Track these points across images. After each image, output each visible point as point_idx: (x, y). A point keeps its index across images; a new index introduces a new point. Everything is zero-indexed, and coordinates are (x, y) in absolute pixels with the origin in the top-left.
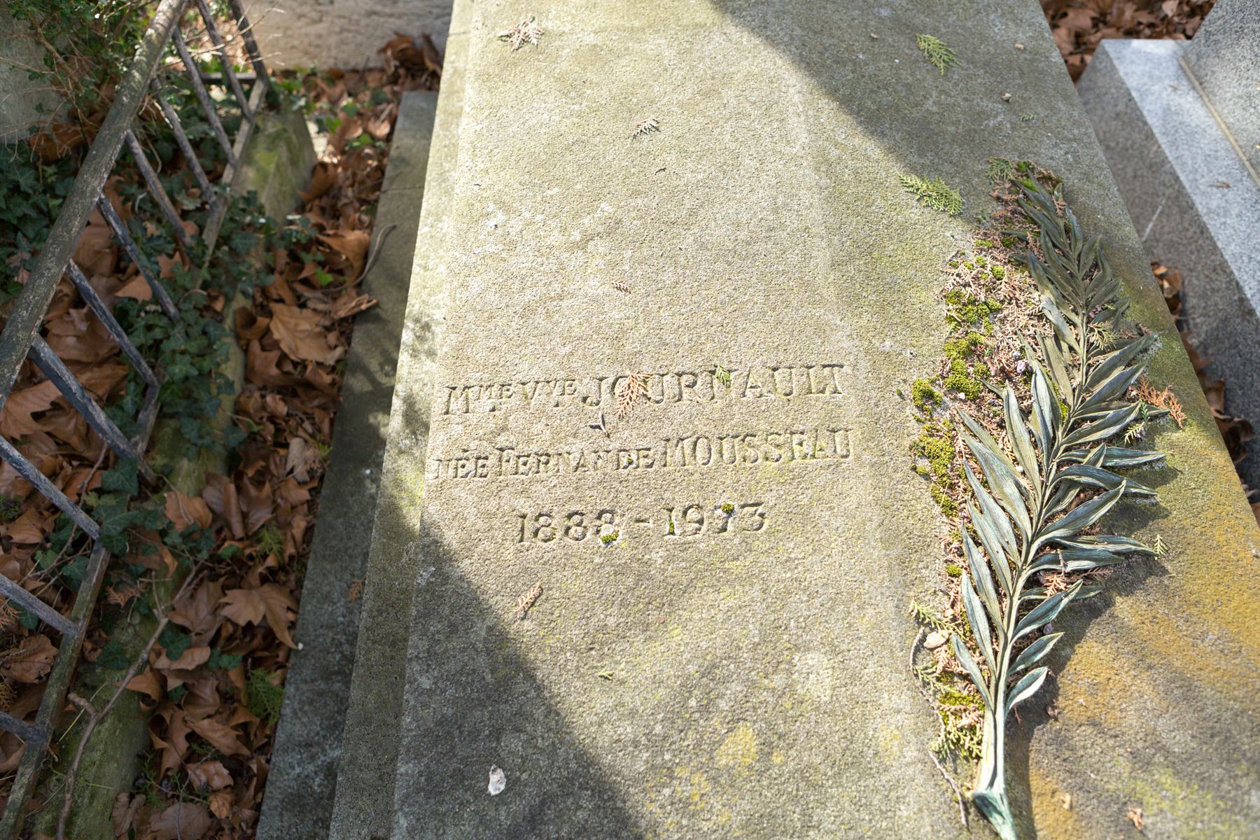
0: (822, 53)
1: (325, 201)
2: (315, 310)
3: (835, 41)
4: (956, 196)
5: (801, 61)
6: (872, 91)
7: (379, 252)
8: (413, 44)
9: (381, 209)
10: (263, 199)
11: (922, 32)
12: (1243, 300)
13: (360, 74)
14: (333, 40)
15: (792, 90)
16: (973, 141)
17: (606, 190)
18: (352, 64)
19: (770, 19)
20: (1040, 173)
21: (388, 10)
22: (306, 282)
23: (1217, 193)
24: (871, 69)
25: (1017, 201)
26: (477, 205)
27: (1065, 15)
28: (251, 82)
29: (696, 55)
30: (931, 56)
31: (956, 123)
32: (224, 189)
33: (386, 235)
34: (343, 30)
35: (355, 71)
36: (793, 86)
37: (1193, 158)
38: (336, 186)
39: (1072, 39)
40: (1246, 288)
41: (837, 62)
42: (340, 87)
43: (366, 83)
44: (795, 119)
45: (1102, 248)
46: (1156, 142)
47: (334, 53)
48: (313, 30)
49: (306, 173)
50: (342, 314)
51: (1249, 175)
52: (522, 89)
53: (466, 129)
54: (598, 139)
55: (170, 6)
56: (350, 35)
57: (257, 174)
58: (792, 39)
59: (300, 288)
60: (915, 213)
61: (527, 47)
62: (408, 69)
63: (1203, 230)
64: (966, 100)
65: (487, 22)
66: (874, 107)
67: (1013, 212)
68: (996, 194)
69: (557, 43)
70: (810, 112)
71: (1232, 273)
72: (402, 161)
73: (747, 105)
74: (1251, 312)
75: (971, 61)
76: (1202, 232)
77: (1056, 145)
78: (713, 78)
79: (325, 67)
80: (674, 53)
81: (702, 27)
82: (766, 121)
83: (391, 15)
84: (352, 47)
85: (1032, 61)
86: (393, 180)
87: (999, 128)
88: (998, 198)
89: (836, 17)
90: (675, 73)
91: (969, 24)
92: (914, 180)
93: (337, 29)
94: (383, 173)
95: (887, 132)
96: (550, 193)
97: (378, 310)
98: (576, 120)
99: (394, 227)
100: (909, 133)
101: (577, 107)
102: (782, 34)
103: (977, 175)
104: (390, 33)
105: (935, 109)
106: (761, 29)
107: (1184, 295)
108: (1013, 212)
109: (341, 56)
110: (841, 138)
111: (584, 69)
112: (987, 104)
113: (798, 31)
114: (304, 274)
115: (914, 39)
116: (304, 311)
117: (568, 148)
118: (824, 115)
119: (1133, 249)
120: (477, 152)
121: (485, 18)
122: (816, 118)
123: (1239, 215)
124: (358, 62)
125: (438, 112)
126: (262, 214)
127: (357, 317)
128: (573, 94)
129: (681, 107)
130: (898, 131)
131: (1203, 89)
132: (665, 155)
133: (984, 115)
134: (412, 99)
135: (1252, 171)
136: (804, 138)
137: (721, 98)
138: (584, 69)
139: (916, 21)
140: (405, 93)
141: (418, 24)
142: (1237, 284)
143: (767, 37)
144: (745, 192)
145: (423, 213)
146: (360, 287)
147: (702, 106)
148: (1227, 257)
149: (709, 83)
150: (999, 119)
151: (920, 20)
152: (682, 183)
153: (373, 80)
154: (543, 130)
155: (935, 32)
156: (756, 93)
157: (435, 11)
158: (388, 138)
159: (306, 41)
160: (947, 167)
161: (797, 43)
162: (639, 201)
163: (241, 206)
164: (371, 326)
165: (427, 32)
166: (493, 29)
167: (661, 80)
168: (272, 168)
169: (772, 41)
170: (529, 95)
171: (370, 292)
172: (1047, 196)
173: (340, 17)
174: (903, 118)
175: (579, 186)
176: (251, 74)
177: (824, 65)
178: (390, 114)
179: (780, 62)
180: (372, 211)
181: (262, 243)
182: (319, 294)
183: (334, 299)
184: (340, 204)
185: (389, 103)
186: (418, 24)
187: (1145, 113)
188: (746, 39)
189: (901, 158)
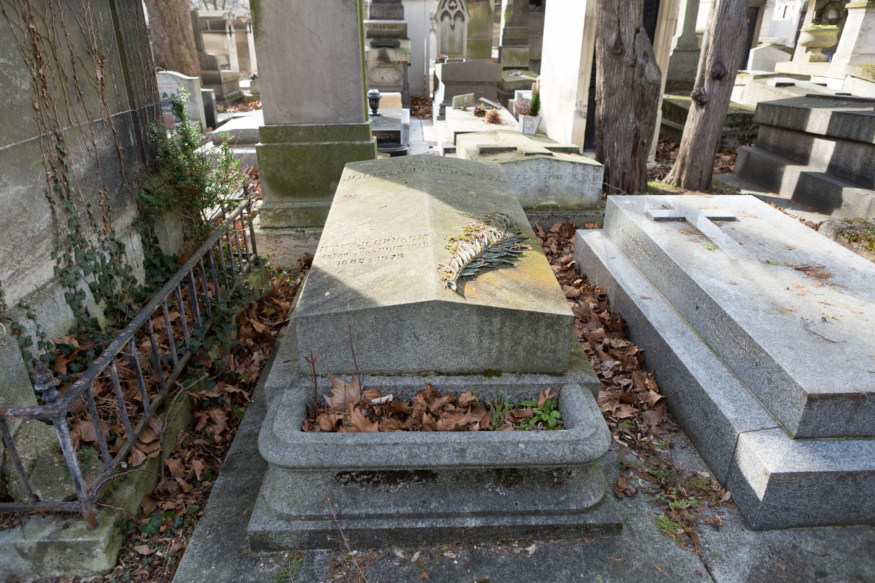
14: (280, 257)
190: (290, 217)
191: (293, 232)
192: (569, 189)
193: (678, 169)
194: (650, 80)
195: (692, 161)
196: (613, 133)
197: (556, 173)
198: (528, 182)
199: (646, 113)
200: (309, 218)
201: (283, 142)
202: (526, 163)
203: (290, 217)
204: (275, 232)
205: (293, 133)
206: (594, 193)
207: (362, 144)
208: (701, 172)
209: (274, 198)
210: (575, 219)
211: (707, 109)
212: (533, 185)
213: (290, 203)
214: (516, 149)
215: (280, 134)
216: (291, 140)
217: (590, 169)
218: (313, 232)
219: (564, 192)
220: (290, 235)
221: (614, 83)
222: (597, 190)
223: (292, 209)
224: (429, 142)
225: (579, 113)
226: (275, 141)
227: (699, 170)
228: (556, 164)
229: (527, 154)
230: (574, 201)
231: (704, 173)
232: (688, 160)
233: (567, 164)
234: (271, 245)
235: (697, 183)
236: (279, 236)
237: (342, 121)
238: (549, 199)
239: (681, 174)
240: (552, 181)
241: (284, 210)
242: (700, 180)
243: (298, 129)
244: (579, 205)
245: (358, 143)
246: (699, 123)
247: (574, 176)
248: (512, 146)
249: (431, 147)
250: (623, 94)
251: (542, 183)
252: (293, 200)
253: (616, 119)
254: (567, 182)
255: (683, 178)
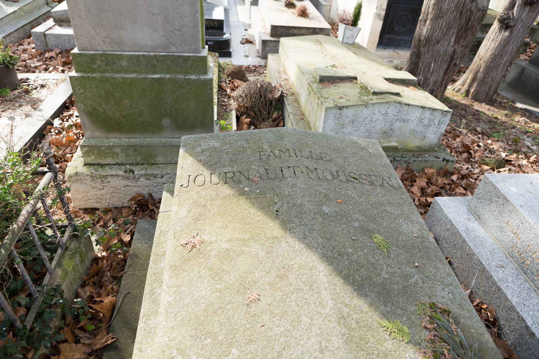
0: (332, 251)
1: (96, 279)
2: (84, 344)
3: (337, 243)
4: (406, 330)
5: (324, 256)
6: (357, 270)
7: (120, 308)
8: (144, 197)
9: (123, 282)
10: (64, 287)
11: (374, 233)
12: (527, 327)
13: (119, 209)
14: (108, 196)
15: (321, 274)
16: (407, 293)
17: (234, 340)
18: (116, 205)
19: (307, 234)
20: (441, 308)
21: (134, 185)
22: (82, 329)
23: (501, 271)
24: (355, 257)
25: (435, 328)
26: (167, 352)
27: (415, 181)
28: (66, 227)
29: (274, 254)
30: (380, 246)
31: (397, 283)
32: (43, 288)
33: (125, 297)
34: (113, 192)
35: (116, 208)
36: (322, 272)
37: (486, 253)
38: (102, 271)
39: (420, 190)
40: (527, 321)
41: (339, 255)
42: (110, 215)
43: (122, 213)
44: (325, 291)
45: (479, 351)
46: (468, 245)
47: (108, 201)
48: (99, 193)
49: (88, 263)
50: (98, 347)
51: (511, 261)
52: (192, 275)
53: (165, 297)
54: (230, 306)
55: (28, 211)
56: (116, 194)
57: (63, 273)
58: (318, 244)
59: (77, 332)
60: (389, 344)
61: (195, 250)
62: (141, 208)
63: (499, 289)
64: (399, 268)
65: (176, 236)
66: (360, 279)
67: (435, 336)
68: (423, 325)
69: (209, 248)
70: (331, 287)
71: (518, 313)
72: (135, 256)
73: (301, 283)
74: (533, 334)
75: (397, 246)
76: (499, 290)
77: (443, 289)
78: (284, 268)
79: (104, 207)
80: (264, 253)
81: (277, 238)
82: (311, 293)
83: (135, 186)
84: (117, 199)
85: (422, 242)
86: (130, 266)
87: (416, 283)
88: (426, 328)
89: (336, 230)
90: (266, 265)
91: (392, 226)
92: (385, 323)
93: (111, 192)
94: (126, 261)
95: (368, 293)
96: (206, 342)
97: (117, 343)
98: (218, 294)
99: (129, 292)
100: (378, 293)
101: (219, 286)
102: (313, 242)
103: (413, 314)
104: (134, 193)
105: (386, 276)
106: (303, 239)
107: (498, 318)
108: (435, 336)
109: (111, 202)
110: (347, 301)
111: (222, 263)
112: (409, 270)
113: (320, 240)
114: (80, 325)
115: (371, 237)
116: (78, 345)
117: (215, 312)
118: (338, 288)
119: (492, 348)
120: (169, 316)
121: (175, 233)
122: (335, 290)
123: (513, 282)
124: (120, 204)
125: (152, 254)
126: (62, 297)
127: (106, 348)
128: (217, 278)
129: (270, 285)
130: (372, 292)
131: (481, 220)
132: (263, 316)
133: (407, 277)
134: (143, 223)
135: (511, 259)
136: (330, 303)
137: (288, 280)
138: (222, 263)
139: (370, 227)
140: (139, 221)
141: (147, 189)
142: (523, 319)
143: (307, 244)
144: (305, 339)
145: (141, 315)
146: (109, 329)
147: (280, 284)
148: (514, 304)
149: (282, 270)
150: (416, 277)
151: (372, 226)
152: (273, 334)
153: (125, 212)
154: (202, 301)
155: (379, 232)
156: (305, 276)
157: (154, 184)
158: (130, 242)
159: (96, 197)
160: (399, 311)
161: (321, 246)
162: (252, 347)
163: (52, 293)
164: (112, 353)
165: (150, 192)
166: (179, 240)
167: (259, 269)
168: (70, 269)
169: (309, 246)
170: (195, 279)
171: (113, 332)
172: (447, 323)
173: (112, 187)
174: (374, 284)
175: (220, 338)
176: (66, 222)
177: (333, 257)
178: (131, 231)
179: (314, 258)
180: (119, 284)
181: (59, 314)
182: (87, 335)
183: (95, 336)
184: (103, 280)
185: (132, 224)
186: (147, 189)
187: (460, 231)
188: (298, 246)
189: (377, 309)
190: (117, 154)
191: (121, 173)
192: (413, 132)
193: (468, 81)
194: (480, 6)
195: (484, 77)
196: (433, 55)
197: (403, 117)
198: (374, 124)
199: (466, 37)
200: (138, 156)
201: (104, 72)
202: (376, 106)
203: (117, 154)
204: (101, 172)
205: (114, 62)
206: (436, 136)
207: (198, 80)
208: (490, 88)
209: (97, 134)
210: (416, 163)
211: (511, 32)
212: (378, 127)
213: (116, 140)
214: (356, 78)
215: (99, 62)
216: (114, 71)
217: (438, 114)
218: (143, 172)
219: (407, 135)
220: (118, 176)
221: (445, 6)
222: (439, 134)
223: (119, 146)
224: (244, 24)
225: (378, 15)
226: (93, 71)
227: (488, 86)
228: (406, 108)
229: (375, 93)
230: (414, 143)
231: (492, 88)
232: (480, 75)
233: (417, 109)
234: (97, 185)
235: (484, 96)
236: (106, 177)
237: (175, 51)
238: (391, 141)
239: (470, 86)
240: (398, 125)
241: (110, 147)
242: (487, 94)
243: (121, 57)
244: (418, 147)
245: (193, 77)
246: (500, 44)
247: (421, 120)
248: (352, 74)
249: (246, 30)
250: (452, 18)
251: (387, 125)
252: (119, 135)
253: (438, 42)
254: (412, 125)
255: (472, 90)
